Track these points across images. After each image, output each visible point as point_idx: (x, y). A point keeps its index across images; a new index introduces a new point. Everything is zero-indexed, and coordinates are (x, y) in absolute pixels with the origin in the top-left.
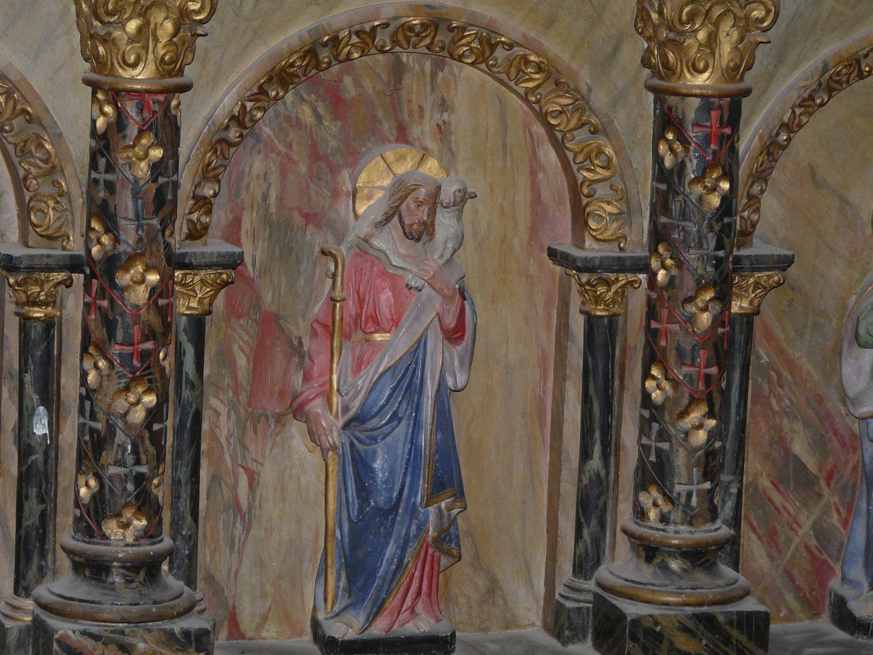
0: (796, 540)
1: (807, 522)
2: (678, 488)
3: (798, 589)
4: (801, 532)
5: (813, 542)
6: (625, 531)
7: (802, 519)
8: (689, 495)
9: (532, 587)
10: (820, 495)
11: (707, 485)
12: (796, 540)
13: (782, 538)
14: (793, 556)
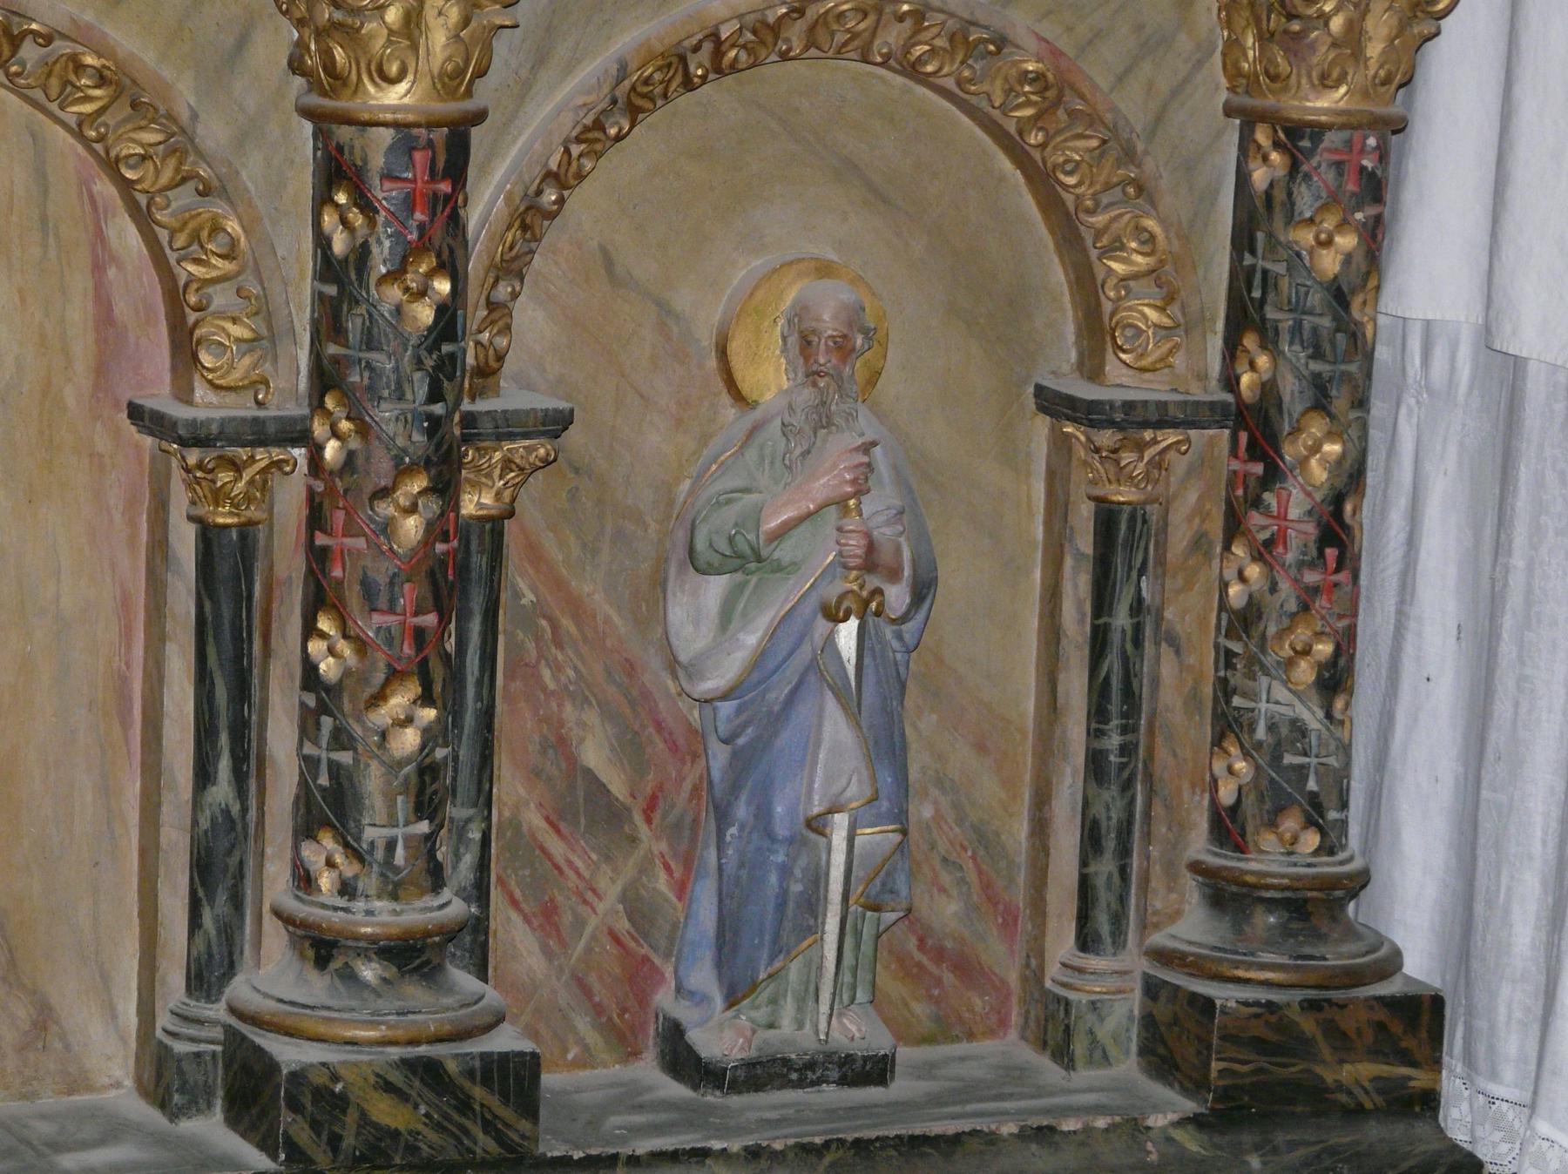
0: (593, 922)
1: (611, 888)
2: (370, 833)
3: (598, 1010)
4: (601, 907)
5: (623, 925)
6: (277, 913)
7: (602, 883)
8: (391, 846)
9: (114, 1017)
10: (633, 840)
11: (424, 827)
12: (593, 922)
13: (567, 919)
14: (589, 950)
